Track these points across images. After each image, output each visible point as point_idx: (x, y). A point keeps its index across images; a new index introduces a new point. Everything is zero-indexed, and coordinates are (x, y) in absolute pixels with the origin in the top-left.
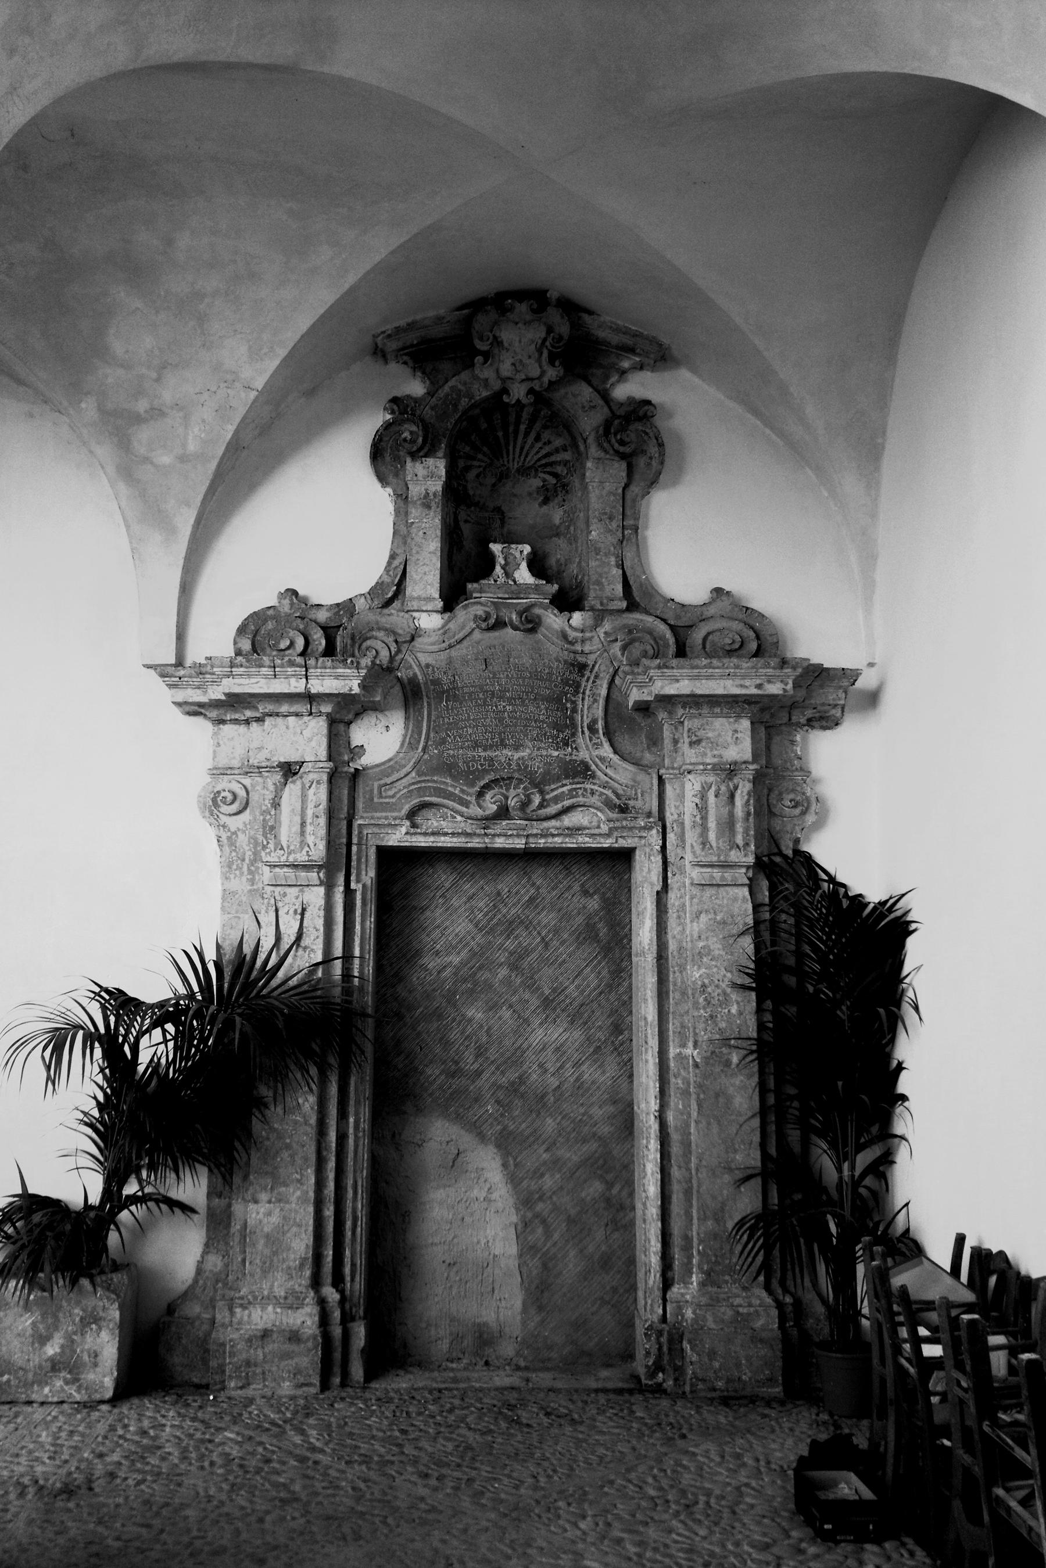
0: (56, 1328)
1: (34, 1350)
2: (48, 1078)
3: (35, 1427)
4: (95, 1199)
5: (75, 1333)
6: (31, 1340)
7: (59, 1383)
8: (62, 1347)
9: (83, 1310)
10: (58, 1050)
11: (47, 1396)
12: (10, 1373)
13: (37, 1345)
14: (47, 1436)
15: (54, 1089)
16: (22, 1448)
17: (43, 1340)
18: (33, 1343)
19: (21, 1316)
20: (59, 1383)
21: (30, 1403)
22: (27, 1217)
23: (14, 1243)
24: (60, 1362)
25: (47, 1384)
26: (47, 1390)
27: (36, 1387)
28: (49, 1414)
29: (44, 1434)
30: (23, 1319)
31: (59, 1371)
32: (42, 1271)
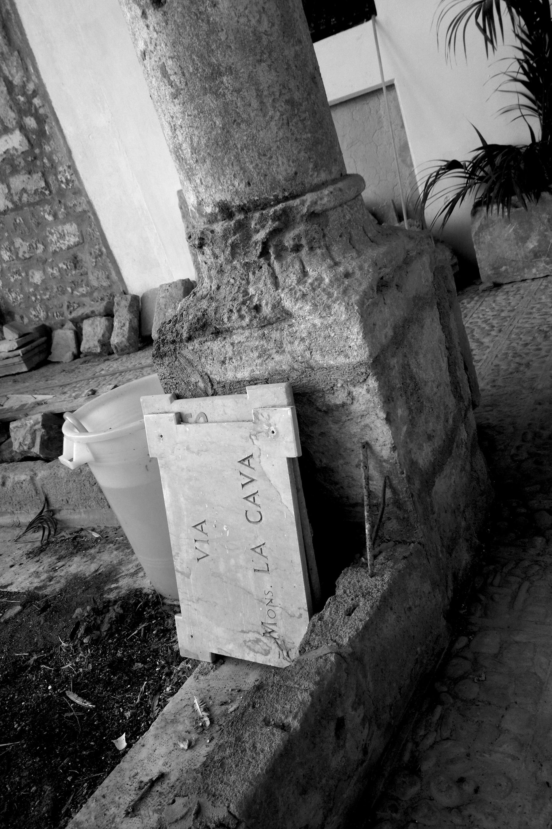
0: (531, 229)
1: (519, 247)
2: (486, 39)
3: (535, 294)
4: (538, 137)
5: (546, 230)
6: (515, 241)
7: (542, 265)
8: (539, 241)
9: (549, 214)
10: (488, 14)
11: (535, 274)
12: (506, 265)
13: (520, 244)
14: (546, 298)
15: (493, 47)
16: (532, 308)
17: (524, 240)
18: (517, 243)
19: (505, 227)
20: (542, 265)
21: (524, 280)
22: (491, 162)
23: (486, 182)
24: (539, 251)
25: (533, 267)
26: (534, 270)
27: (526, 270)
28: (541, 285)
29: (543, 297)
30: (506, 229)
31: (540, 256)
32: (514, 194)
